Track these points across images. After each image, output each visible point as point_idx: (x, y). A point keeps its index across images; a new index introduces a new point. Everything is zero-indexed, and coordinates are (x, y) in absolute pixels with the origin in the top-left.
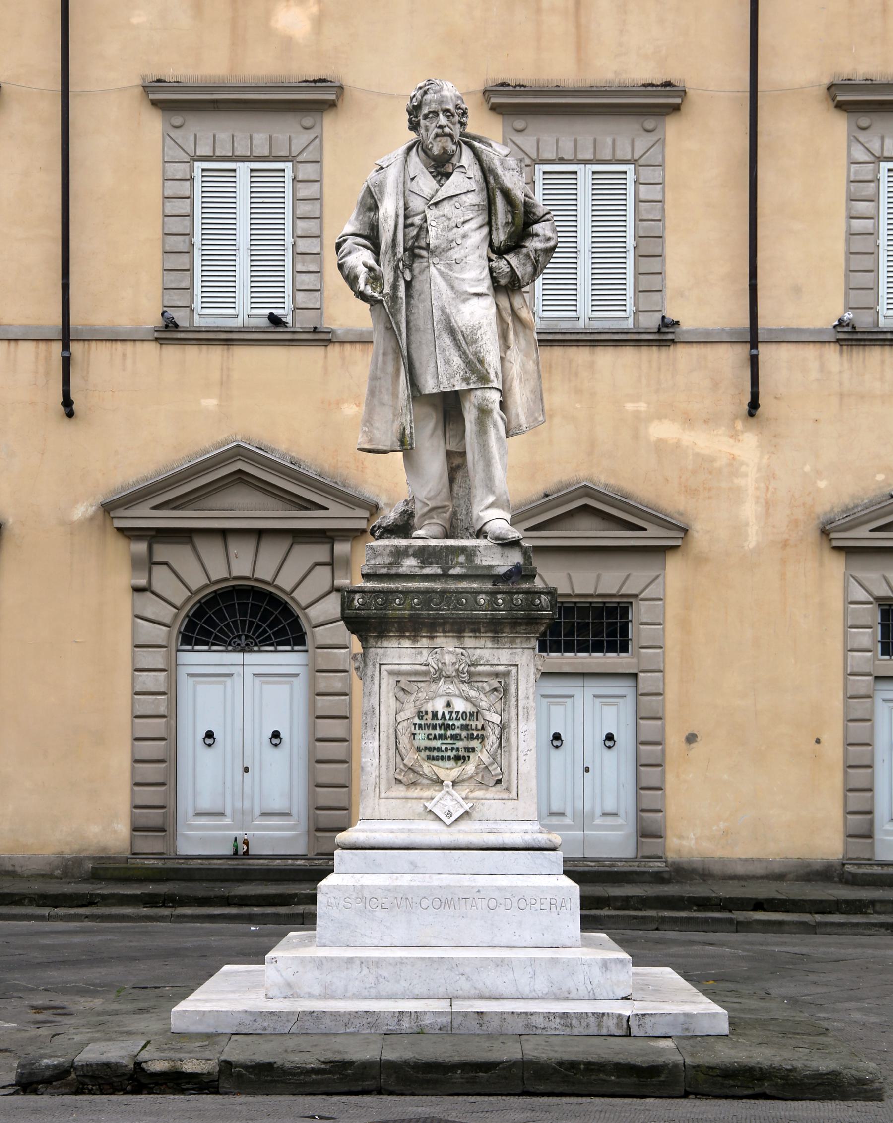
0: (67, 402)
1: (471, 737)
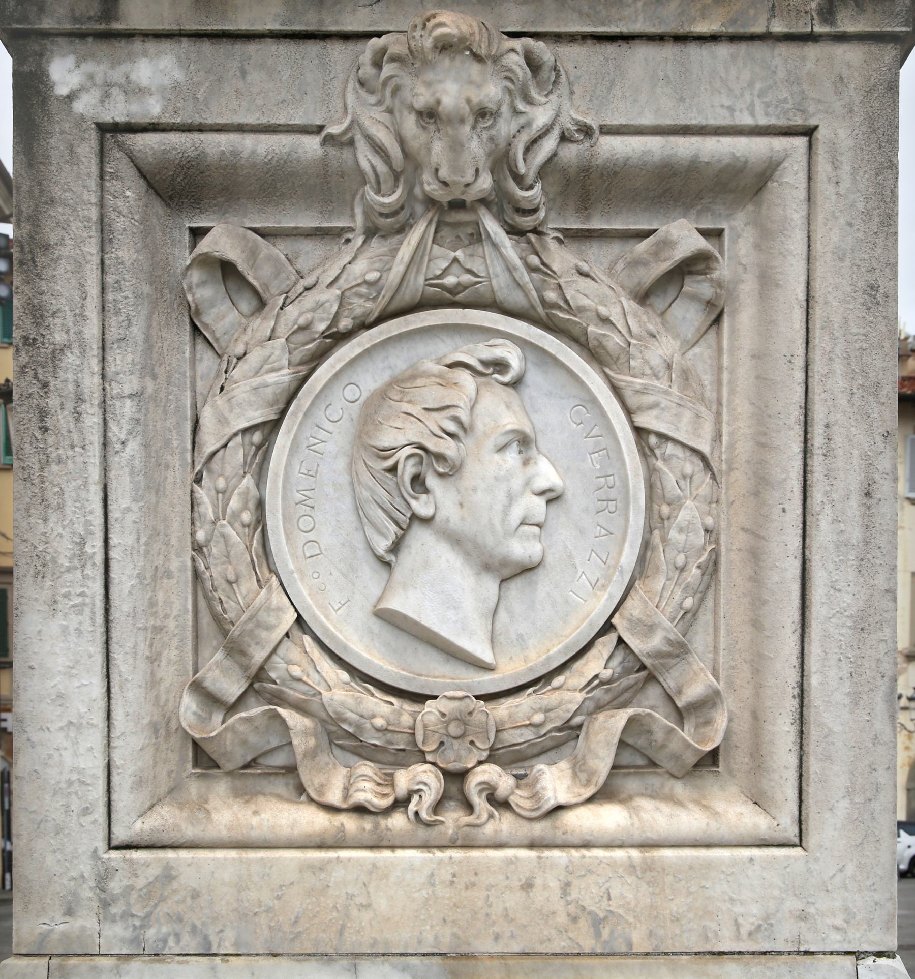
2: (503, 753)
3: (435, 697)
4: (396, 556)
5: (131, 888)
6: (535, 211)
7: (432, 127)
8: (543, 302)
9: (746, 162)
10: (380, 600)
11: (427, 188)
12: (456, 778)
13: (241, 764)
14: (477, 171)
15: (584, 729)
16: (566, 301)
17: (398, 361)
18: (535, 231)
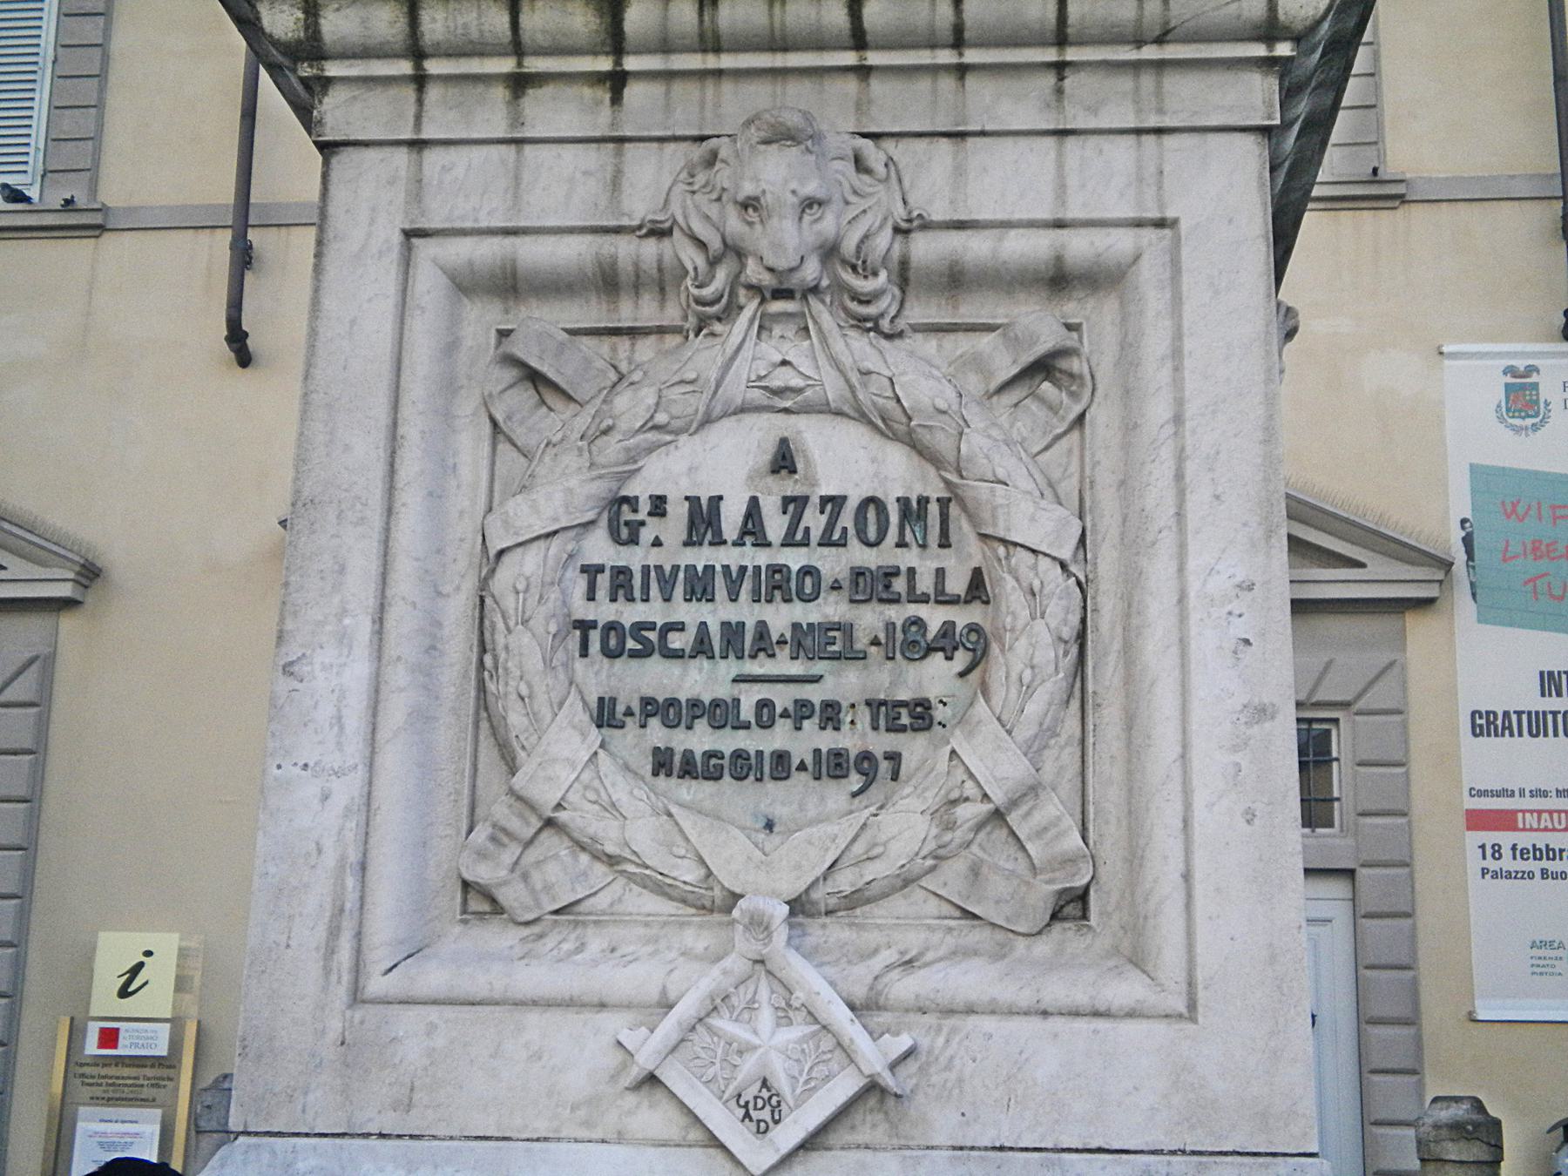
0: (237, 338)
1: (913, 644)
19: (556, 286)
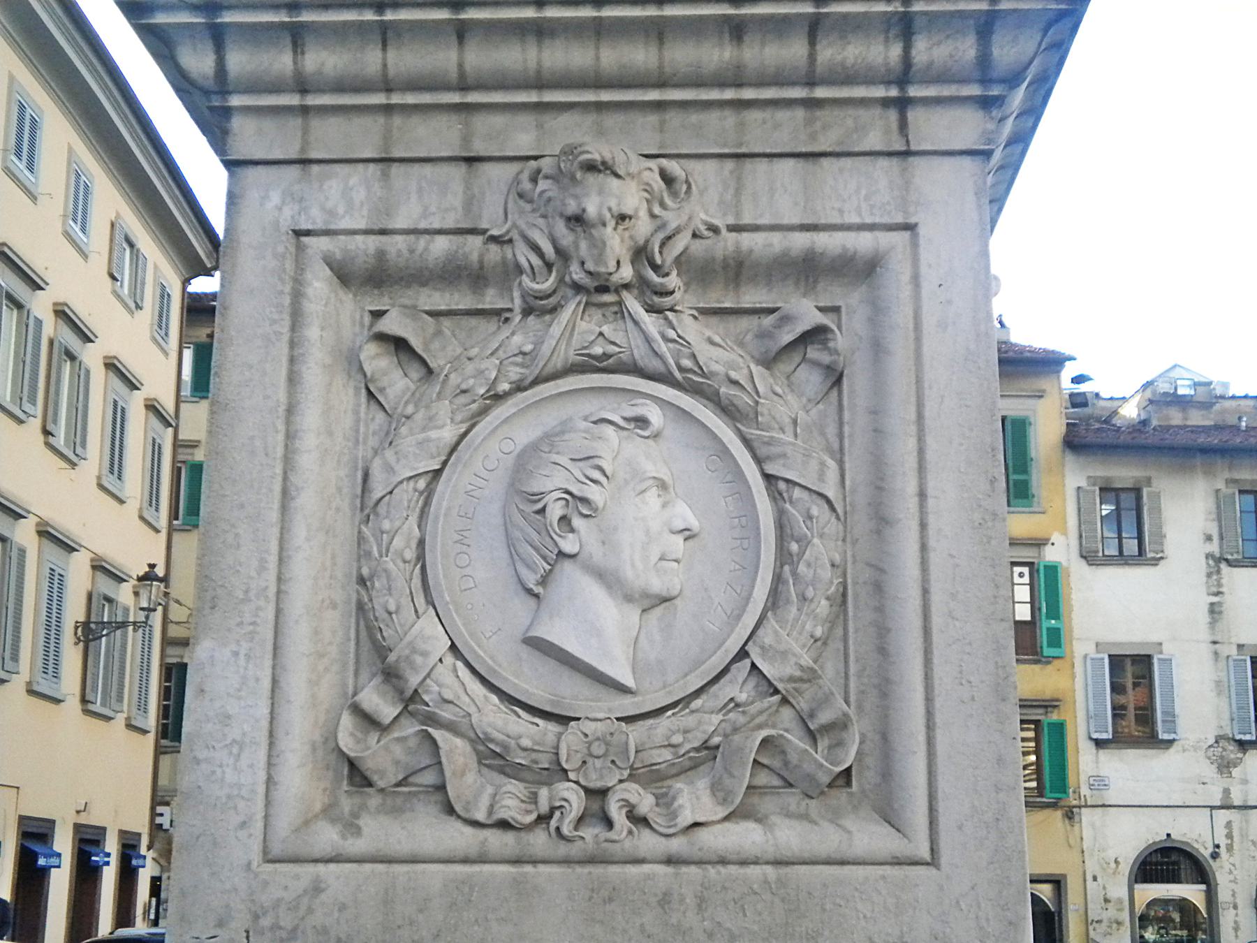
2: (643, 773)
3: (578, 719)
4: (544, 588)
5: (279, 900)
6: (672, 293)
7: (579, 229)
8: (681, 369)
9: (855, 253)
10: (528, 630)
11: (575, 277)
12: (599, 794)
13: (394, 782)
14: (618, 262)
15: (721, 749)
16: (701, 368)
17: (549, 418)
18: (672, 310)
19: (420, 277)
